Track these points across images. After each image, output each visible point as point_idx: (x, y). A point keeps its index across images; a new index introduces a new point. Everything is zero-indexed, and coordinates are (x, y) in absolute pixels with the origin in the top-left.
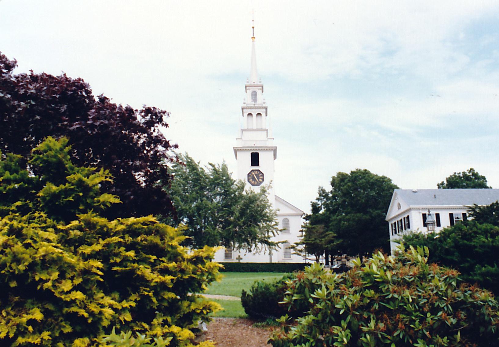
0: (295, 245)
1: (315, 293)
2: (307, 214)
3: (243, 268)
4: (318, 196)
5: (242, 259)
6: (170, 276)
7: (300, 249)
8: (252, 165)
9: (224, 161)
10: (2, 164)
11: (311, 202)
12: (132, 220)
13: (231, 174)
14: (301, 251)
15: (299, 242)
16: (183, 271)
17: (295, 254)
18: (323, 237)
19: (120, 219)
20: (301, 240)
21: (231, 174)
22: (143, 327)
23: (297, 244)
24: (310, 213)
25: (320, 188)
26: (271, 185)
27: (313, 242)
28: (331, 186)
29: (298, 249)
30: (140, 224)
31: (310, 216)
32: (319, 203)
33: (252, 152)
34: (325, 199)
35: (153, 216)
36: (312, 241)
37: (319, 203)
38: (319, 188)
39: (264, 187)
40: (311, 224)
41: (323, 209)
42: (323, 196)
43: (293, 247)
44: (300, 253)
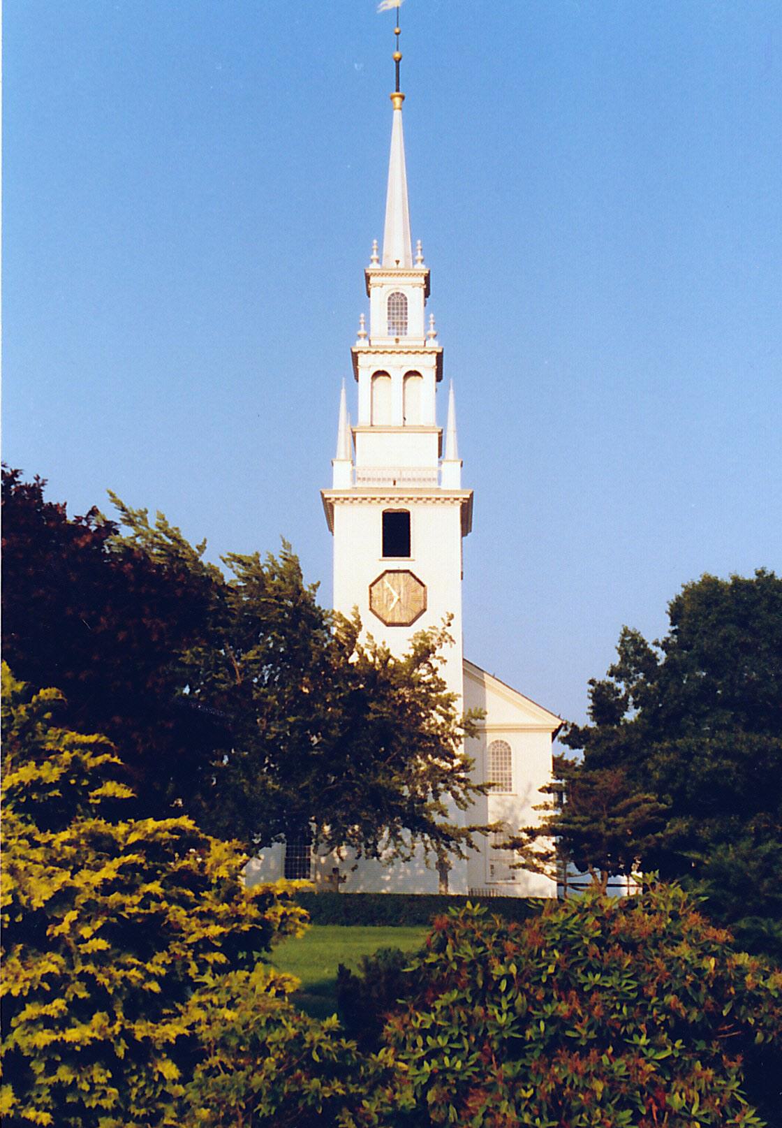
0: (525, 836)
1: (461, 950)
2: (574, 726)
3: (347, 911)
4: (616, 660)
5: (343, 880)
6: (218, 926)
7: (543, 851)
8: (384, 555)
9: (287, 546)
10: (43, 770)
11: (592, 682)
12: (151, 824)
13: (315, 587)
14: (545, 857)
15: (537, 825)
16: (240, 919)
17: (524, 866)
18: (624, 813)
19: (132, 821)
20: (545, 818)
21: (315, 587)
22: (177, 1009)
23: (533, 833)
24: (585, 721)
25: (626, 633)
26: (448, 629)
27: (584, 829)
28: (669, 620)
29: (535, 851)
30: (167, 833)
31: (587, 731)
32: (621, 686)
33: (385, 506)
34: (641, 676)
35: (189, 818)
36: (583, 824)
37: (621, 686)
38: (624, 635)
39: (425, 638)
40: (590, 762)
41: (631, 707)
42: (635, 663)
43: (516, 844)
44: (541, 865)
